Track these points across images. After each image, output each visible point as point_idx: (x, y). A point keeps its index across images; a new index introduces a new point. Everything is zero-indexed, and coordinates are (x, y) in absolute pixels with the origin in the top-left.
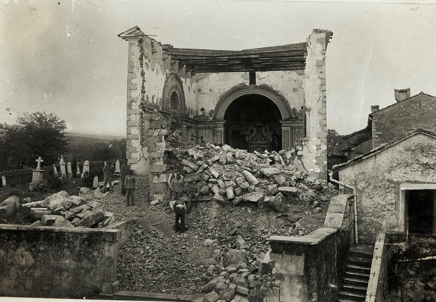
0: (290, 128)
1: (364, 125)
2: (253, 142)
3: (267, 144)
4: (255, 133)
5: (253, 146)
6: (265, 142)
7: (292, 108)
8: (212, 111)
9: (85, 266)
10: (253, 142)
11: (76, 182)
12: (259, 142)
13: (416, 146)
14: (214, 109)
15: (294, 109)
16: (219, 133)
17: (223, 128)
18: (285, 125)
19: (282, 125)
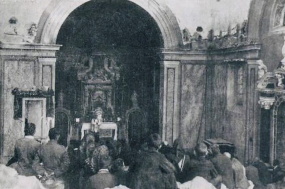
0: (178, 63)
1: (245, 17)
2: (90, 81)
3: (110, 84)
4: (91, 66)
5: (90, 86)
6: (108, 81)
7: (182, 28)
8: (35, 25)
9: (80, 177)
10: (90, 81)
11: (119, 116)
12: (99, 81)
13: (59, 166)
14: (36, 22)
15: (184, 31)
16: (47, 69)
17: (55, 60)
18: (169, 57)
19: (166, 57)
